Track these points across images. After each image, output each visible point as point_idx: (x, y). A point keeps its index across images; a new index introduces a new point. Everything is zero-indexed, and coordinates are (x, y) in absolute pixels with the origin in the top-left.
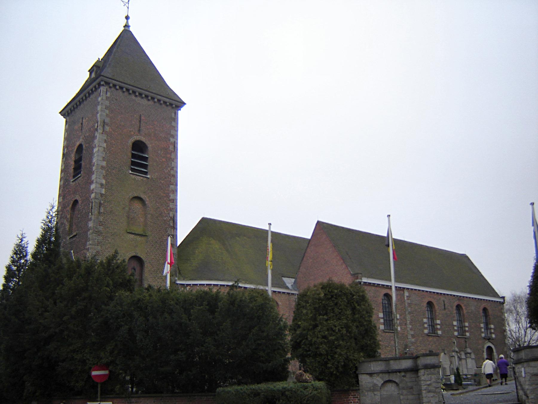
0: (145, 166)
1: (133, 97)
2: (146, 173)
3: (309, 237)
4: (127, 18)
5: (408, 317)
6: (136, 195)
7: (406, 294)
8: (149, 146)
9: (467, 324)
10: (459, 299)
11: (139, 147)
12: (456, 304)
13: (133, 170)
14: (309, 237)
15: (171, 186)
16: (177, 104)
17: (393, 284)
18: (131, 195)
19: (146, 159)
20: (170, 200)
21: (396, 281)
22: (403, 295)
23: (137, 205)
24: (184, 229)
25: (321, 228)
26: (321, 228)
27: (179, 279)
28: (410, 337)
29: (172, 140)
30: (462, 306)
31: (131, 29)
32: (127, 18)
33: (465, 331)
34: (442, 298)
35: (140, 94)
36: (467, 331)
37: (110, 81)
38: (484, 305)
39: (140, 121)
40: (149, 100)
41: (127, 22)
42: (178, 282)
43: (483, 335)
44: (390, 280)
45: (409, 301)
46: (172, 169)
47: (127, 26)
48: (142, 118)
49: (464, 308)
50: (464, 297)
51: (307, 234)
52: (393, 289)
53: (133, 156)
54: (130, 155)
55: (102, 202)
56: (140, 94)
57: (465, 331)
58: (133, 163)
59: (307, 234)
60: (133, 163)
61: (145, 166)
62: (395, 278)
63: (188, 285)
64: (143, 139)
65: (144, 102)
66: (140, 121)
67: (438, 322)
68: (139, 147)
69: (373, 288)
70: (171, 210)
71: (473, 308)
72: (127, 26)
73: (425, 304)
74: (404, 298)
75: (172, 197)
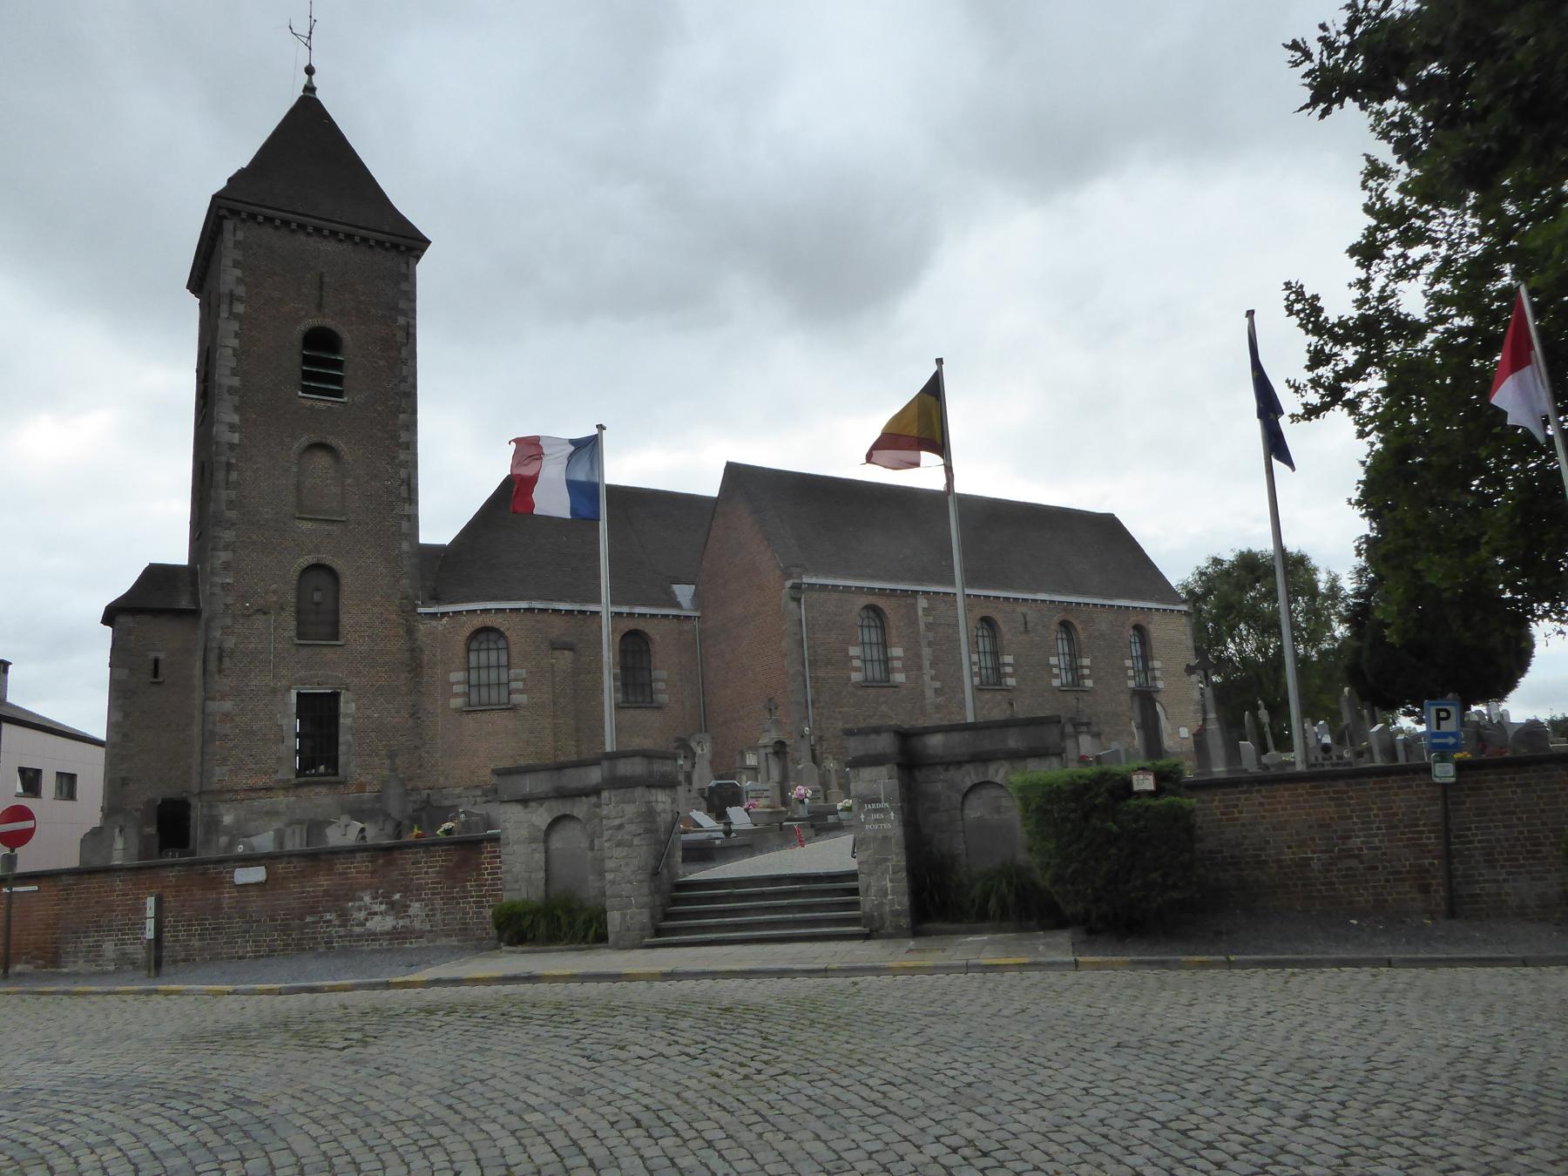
0: (338, 380)
1: (302, 237)
2: (339, 394)
3: (714, 493)
4: (310, 71)
5: (926, 652)
6: (316, 440)
7: (922, 603)
8: (346, 337)
9: (1086, 662)
10: (1065, 609)
11: (321, 343)
12: (1058, 618)
13: (306, 389)
14: (714, 493)
15: (402, 416)
16: (412, 243)
17: (957, 589)
18: (304, 440)
19: (338, 365)
20: (399, 445)
21: (970, 581)
22: (914, 607)
23: (322, 460)
24: (446, 505)
25: (736, 475)
26: (736, 475)
27: (424, 605)
28: (929, 693)
29: (402, 320)
30: (1075, 622)
31: (319, 95)
32: (310, 71)
33: (1083, 677)
34: (1021, 609)
35: (318, 230)
36: (1088, 677)
37: (257, 209)
38: (1134, 619)
39: (321, 288)
40: (340, 241)
41: (310, 80)
42: (420, 610)
43: (1131, 684)
44: (952, 583)
45: (930, 619)
46: (404, 380)
47: (310, 88)
48: (326, 279)
49: (1079, 627)
50: (1078, 604)
51: (710, 487)
52: (960, 599)
53: (307, 360)
54: (299, 359)
55: (233, 461)
56: (318, 230)
57: (1083, 677)
58: (307, 376)
59: (710, 487)
60: (307, 376)
61: (338, 380)
62: (966, 570)
63: (444, 614)
64: (329, 323)
65: (329, 246)
66: (321, 288)
67: (1008, 659)
68: (321, 343)
69: (835, 595)
70: (404, 464)
71: (1104, 627)
72: (310, 88)
73: (1054, 626)
74: (916, 613)
75: (404, 436)
